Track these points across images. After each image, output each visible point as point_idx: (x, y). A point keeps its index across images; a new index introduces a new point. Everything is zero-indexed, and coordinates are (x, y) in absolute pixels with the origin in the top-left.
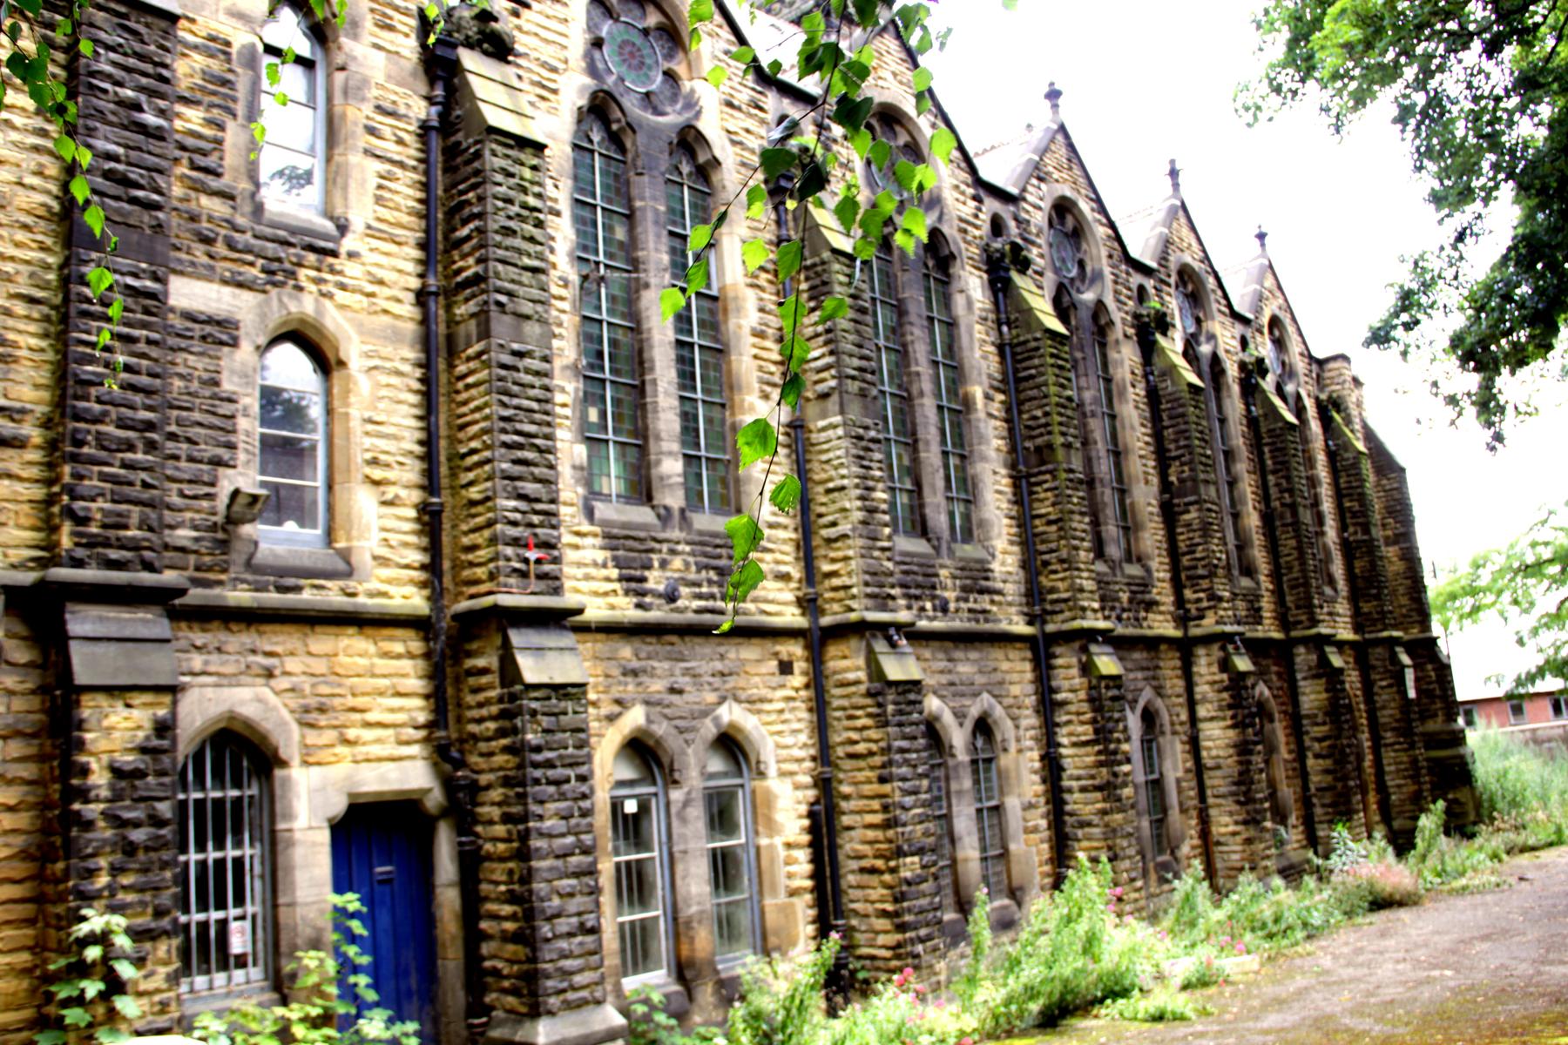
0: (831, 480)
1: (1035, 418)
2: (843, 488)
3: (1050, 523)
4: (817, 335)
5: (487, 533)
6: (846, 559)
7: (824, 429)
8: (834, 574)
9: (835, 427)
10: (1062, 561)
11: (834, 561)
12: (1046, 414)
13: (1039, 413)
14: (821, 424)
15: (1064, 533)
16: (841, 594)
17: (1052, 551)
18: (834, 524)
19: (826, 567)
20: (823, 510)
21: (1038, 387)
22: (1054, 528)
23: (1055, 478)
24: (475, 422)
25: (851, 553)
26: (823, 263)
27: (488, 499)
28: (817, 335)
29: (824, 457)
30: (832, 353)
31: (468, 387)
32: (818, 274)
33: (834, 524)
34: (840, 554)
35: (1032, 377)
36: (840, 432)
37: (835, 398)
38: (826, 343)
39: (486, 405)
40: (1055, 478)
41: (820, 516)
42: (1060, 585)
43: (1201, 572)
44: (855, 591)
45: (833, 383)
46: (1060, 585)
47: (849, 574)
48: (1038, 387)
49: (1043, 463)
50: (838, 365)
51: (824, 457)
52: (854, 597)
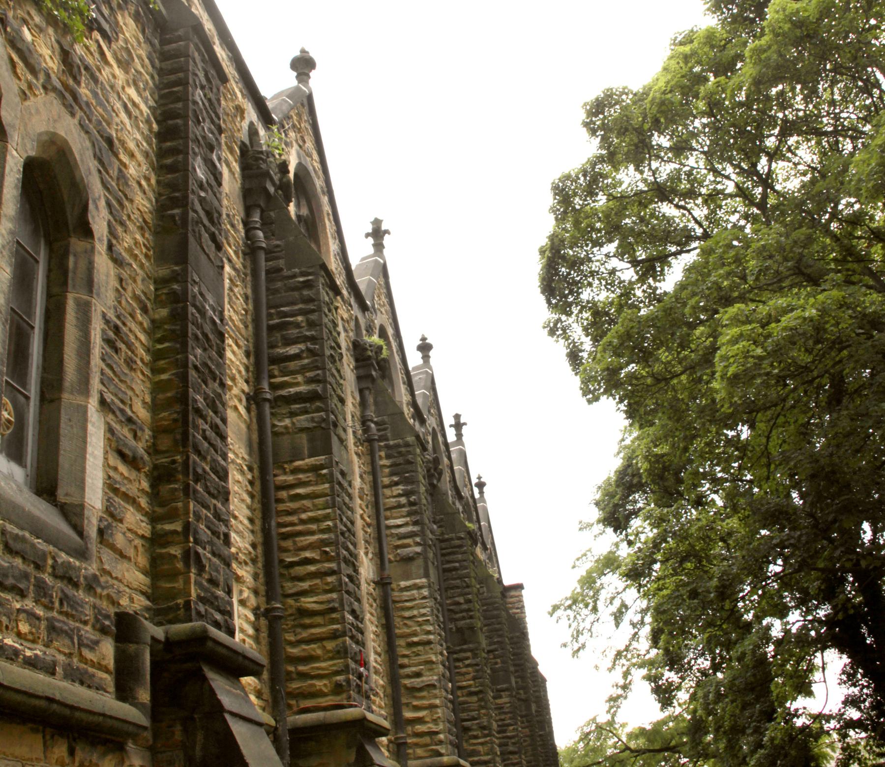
0: (415, 634)
1: (459, 604)
2: (429, 642)
3: (471, 694)
4: (400, 506)
5: (330, 645)
6: (432, 707)
7: (407, 589)
8: (420, 721)
9: (419, 588)
10: (483, 728)
11: (417, 708)
12: (469, 601)
13: (461, 600)
14: (403, 584)
15: (744, 654)
16: (427, 739)
17: (474, 719)
18: (418, 675)
19: (408, 714)
20: (406, 661)
21: (461, 578)
22: (475, 698)
23: (475, 656)
24: (312, 533)
25: (437, 702)
26: (407, 445)
27: (333, 610)
28: (400, 506)
29: (407, 614)
30: (415, 523)
31: (298, 497)
32: (400, 454)
33: (418, 675)
34: (426, 702)
35: (455, 569)
36: (425, 592)
37: (420, 561)
38: (409, 514)
39: (326, 517)
40: (475, 656)
41: (403, 666)
42: (480, 748)
43: (511, 748)
44: (442, 736)
45: (418, 549)
46: (480, 748)
47: (435, 721)
48: (461, 578)
49: (465, 642)
50: (422, 533)
51: (407, 614)
52: (441, 742)
